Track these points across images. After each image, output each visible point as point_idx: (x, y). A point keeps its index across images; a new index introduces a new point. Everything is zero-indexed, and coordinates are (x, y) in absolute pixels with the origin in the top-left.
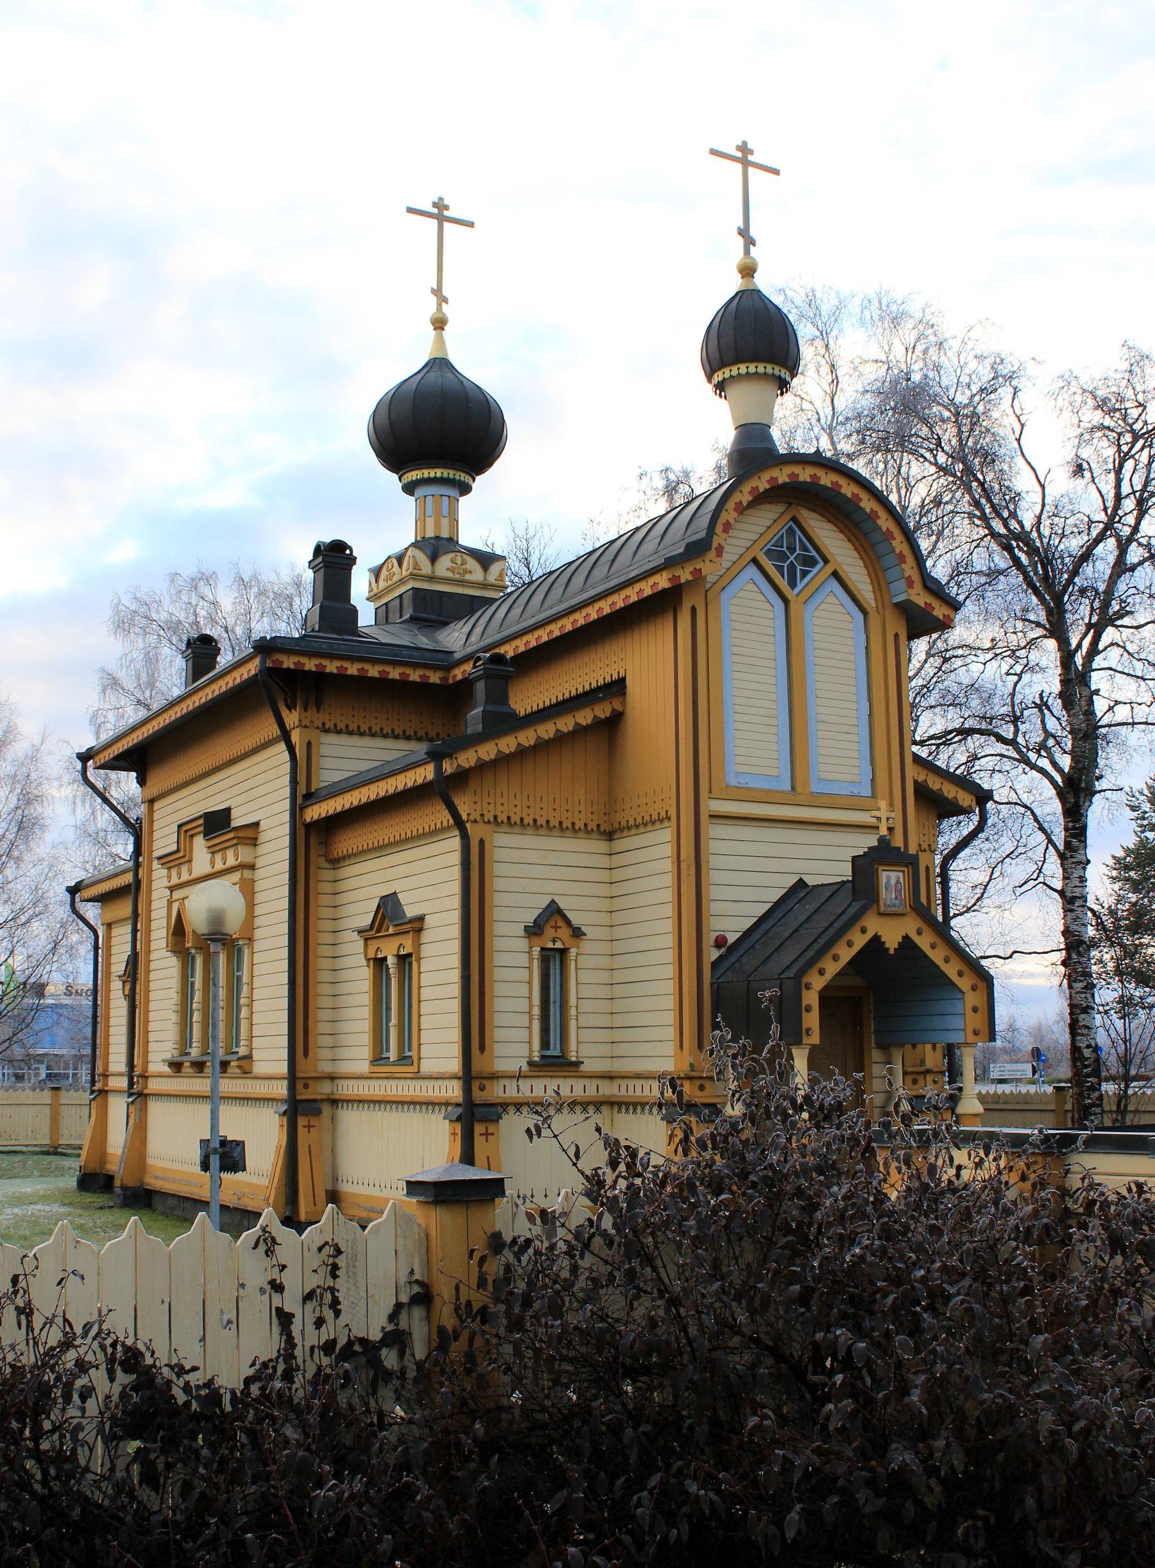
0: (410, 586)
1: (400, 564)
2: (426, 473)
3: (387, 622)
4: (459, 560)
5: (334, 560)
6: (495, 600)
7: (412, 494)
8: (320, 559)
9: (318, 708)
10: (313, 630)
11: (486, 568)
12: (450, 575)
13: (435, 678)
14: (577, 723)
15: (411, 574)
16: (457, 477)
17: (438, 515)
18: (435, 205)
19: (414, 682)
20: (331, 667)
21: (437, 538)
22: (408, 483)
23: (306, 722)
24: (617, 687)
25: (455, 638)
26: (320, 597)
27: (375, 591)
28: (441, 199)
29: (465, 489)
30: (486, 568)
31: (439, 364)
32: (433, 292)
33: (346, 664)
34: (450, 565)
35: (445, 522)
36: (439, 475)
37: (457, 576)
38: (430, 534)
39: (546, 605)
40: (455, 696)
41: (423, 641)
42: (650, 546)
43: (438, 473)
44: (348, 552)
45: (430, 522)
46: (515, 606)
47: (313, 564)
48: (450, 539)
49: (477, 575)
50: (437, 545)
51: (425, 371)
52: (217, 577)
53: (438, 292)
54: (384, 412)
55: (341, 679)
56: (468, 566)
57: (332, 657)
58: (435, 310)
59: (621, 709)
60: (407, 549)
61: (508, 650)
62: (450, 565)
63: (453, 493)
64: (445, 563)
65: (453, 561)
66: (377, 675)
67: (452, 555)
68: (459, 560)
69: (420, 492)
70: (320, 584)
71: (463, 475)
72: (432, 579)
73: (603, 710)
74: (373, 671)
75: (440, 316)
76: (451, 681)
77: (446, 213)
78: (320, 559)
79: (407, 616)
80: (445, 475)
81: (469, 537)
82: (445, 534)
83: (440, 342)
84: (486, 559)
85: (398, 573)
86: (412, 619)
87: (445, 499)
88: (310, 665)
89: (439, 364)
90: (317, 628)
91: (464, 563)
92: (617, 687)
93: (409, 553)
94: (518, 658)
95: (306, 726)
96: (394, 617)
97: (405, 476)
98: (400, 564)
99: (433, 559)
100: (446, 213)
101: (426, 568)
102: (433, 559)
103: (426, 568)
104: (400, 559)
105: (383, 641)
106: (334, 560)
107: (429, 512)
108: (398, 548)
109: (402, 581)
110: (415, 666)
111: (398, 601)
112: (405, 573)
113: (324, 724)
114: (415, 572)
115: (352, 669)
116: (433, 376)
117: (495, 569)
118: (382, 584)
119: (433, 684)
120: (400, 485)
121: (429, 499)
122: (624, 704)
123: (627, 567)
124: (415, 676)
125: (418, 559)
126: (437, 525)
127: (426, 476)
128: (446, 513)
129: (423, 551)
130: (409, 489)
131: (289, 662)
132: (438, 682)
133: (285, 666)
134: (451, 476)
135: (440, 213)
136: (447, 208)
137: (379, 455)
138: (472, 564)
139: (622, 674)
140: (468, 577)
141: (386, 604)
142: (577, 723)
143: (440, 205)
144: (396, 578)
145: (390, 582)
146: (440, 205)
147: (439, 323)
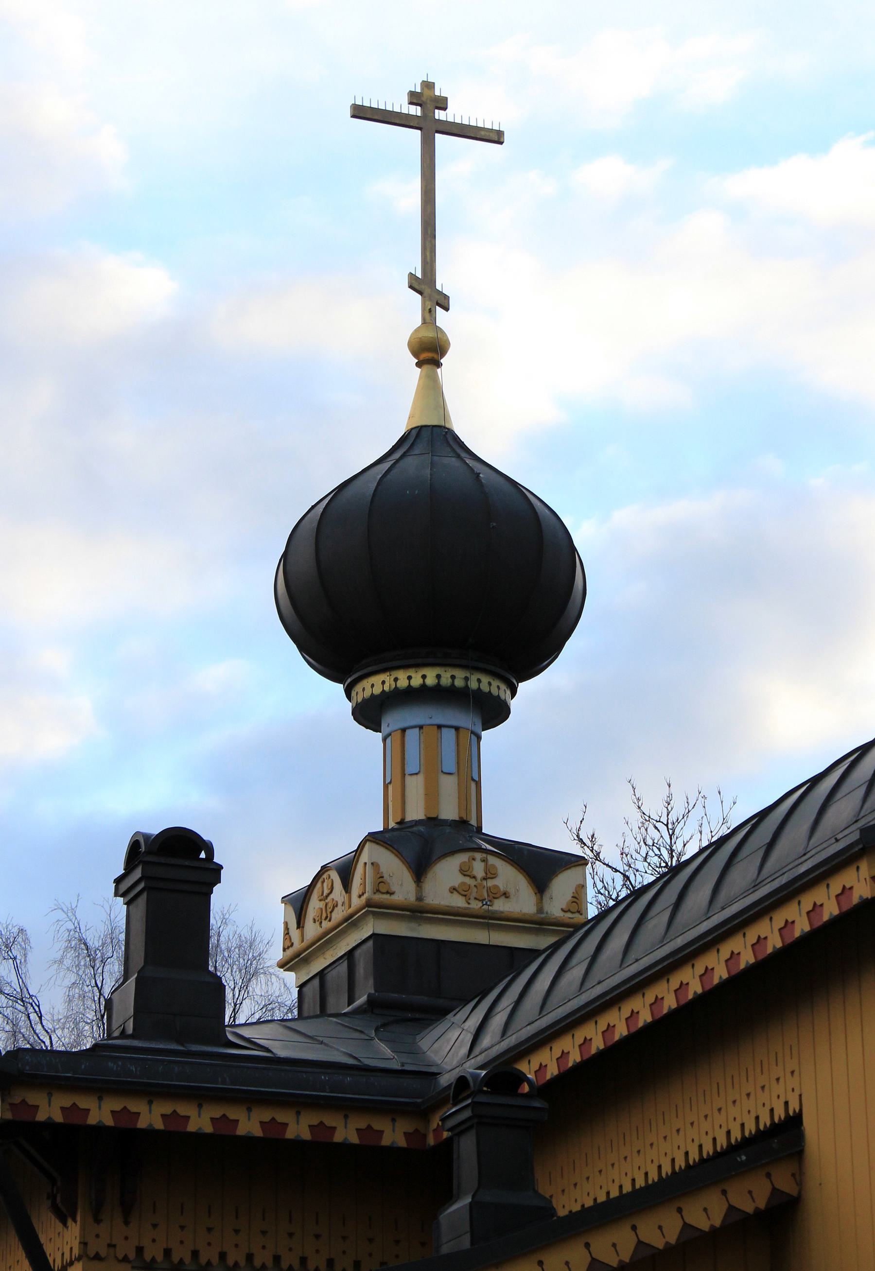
0: (366, 931)
1: (347, 885)
2: (403, 679)
3: (323, 1011)
4: (478, 869)
5: (170, 873)
6: (534, 953)
7: (375, 727)
8: (137, 874)
9: (127, 1212)
10: (123, 1035)
11: (540, 886)
12: (458, 902)
13: (394, 1134)
14: (686, 1226)
15: (369, 904)
16: (473, 685)
17: (432, 771)
18: (414, 98)
19: (345, 1146)
20: (151, 1116)
21: (432, 821)
22: (365, 701)
23: (98, 1246)
24: (784, 1138)
25: (453, 1047)
26: (138, 960)
27: (297, 946)
28: (428, 85)
29: (495, 713)
30: (540, 886)
31: (432, 438)
32: (415, 284)
33: (184, 1109)
34: (458, 879)
35: (449, 786)
36: (431, 681)
37: (475, 905)
38: (416, 812)
39: (632, 956)
40: (425, 1175)
41: (383, 1053)
42: (843, 810)
43: (431, 676)
44: (203, 855)
45: (415, 787)
46: (574, 961)
47: (124, 887)
48: (462, 823)
49: (521, 900)
50: (424, 838)
51: (397, 455)
52: (26, 940)
53: (424, 285)
54: (306, 551)
55: (173, 1141)
56: (500, 882)
57: (152, 1092)
58: (418, 322)
59: (795, 1193)
60: (361, 846)
61: (541, 1066)
62: (458, 879)
63: (466, 720)
64: (445, 880)
65: (465, 871)
66: (258, 1132)
67: (463, 858)
68: (478, 869)
69: (393, 720)
70: (139, 926)
71: (485, 679)
72: (418, 912)
73: (750, 1194)
74: (249, 1124)
75: (430, 334)
76: (431, 1141)
77: (440, 115)
78: (137, 874)
79: (361, 1000)
80: (446, 681)
81: (505, 817)
82: (449, 812)
83: (432, 391)
84: (541, 866)
85: (345, 902)
86: (373, 1004)
87: (449, 736)
88: (101, 1112)
89: (432, 438)
90: (130, 1030)
91: (490, 874)
92: (784, 1138)
93: (364, 857)
94: (570, 1078)
95: (97, 1257)
96: (339, 1003)
97: (358, 688)
98: (347, 885)
99: (420, 869)
100: (440, 115)
101: (404, 889)
102: (420, 869)
103: (404, 889)
104: (345, 870)
105: (282, 1053)
106: (170, 873)
107: (412, 765)
108: (342, 847)
109: (351, 922)
110: (347, 1107)
111: (344, 967)
112: (356, 902)
113: (140, 1250)
114: (379, 897)
115: (200, 1120)
116: (415, 465)
117: (561, 887)
118: (312, 930)
119: (391, 1150)
120: (348, 706)
121: (412, 736)
122: (799, 1177)
123: (795, 852)
124: (346, 1131)
125: (384, 869)
126: (432, 794)
127: (403, 683)
128: (449, 764)
129: (399, 854)
130: (368, 714)
131: (50, 1108)
132: (402, 1143)
133: (41, 1117)
134: (459, 683)
135: (426, 115)
136: (442, 104)
137: (304, 648)
138: (508, 876)
139: (794, 1106)
140: (500, 906)
141: (321, 974)
142: (686, 1226)
143: (427, 99)
144: (338, 915)
145: (326, 925)
146: (427, 99)
147: (430, 351)
